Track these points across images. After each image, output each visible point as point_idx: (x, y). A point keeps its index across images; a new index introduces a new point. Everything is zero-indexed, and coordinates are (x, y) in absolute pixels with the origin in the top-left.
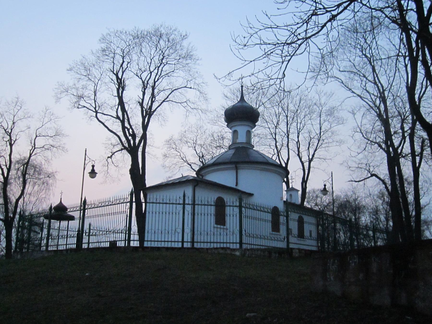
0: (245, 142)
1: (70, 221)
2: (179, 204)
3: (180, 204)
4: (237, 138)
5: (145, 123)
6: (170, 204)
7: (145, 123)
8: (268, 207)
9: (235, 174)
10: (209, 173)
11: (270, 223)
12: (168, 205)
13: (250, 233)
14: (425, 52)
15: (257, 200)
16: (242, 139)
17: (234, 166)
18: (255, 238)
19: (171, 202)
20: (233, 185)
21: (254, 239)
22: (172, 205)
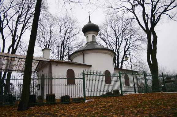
0: (92, 41)
1: (25, 60)
2: (81, 78)
3: (82, 78)
4: (88, 40)
5: (2, 78)
6: (63, 79)
7: (2, 78)
8: (97, 72)
9: (83, 58)
10: (75, 57)
11: (112, 80)
12: (58, 80)
13: (92, 89)
14: (3, 76)
15: (94, 69)
16: (90, 40)
17: (82, 53)
18: (102, 92)
19: (60, 78)
20: (82, 63)
21: (99, 93)
22: (65, 79)
